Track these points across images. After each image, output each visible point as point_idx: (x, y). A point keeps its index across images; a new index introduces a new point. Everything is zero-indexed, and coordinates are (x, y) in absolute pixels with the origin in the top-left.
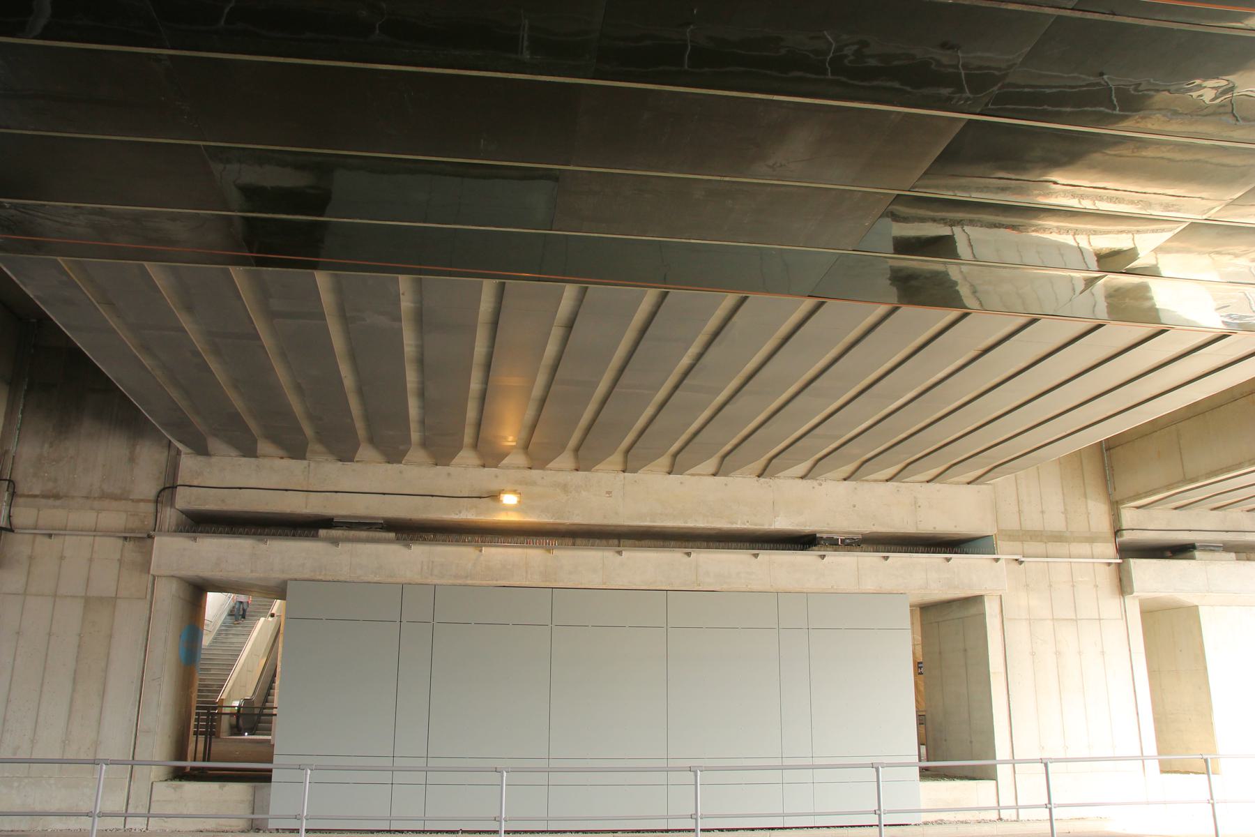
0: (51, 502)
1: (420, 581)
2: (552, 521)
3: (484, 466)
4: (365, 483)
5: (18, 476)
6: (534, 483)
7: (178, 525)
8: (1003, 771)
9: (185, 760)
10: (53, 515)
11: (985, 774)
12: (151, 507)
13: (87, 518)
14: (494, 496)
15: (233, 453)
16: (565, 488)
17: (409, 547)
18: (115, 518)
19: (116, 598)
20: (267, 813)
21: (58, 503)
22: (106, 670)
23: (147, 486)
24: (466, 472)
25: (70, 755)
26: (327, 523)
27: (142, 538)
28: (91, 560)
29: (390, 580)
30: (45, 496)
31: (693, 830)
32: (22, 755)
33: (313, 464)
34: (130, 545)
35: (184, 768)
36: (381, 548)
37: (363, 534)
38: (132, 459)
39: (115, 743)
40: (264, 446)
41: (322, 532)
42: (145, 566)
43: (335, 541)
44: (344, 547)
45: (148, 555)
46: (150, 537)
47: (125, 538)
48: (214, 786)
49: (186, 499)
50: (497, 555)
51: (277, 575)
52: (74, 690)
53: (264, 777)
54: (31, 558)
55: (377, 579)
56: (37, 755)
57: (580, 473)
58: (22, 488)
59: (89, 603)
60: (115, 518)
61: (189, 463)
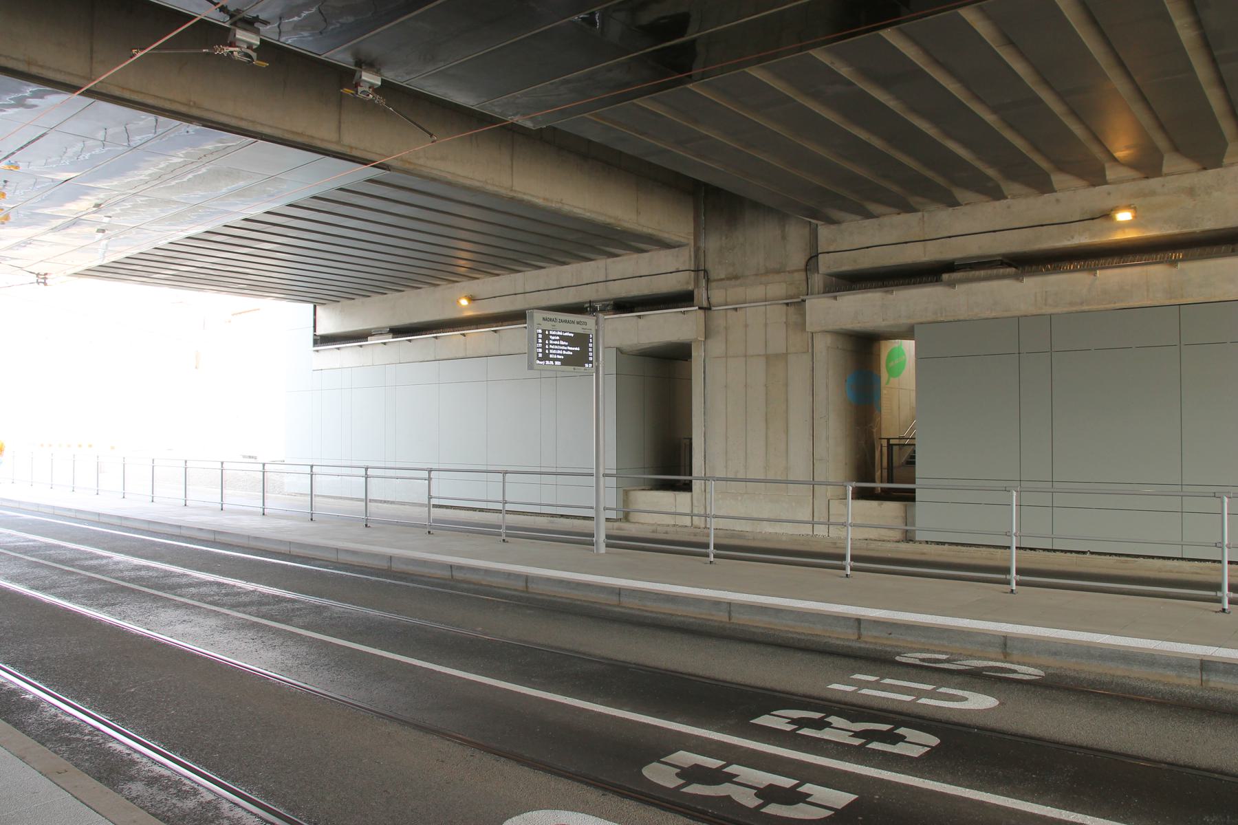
0: (733, 282)
1: (1035, 312)
2: (1176, 231)
3: (1205, 169)
4: (972, 226)
5: (709, 266)
6: (1153, 193)
7: (825, 287)
8: (697, 485)
9: (874, 481)
10: (737, 292)
11: (687, 487)
12: (802, 276)
13: (758, 291)
14: (1107, 215)
15: (858, 218)
16: (1191, 192)
17: (1022, 281)
18: (777, 288)
19: (787, 354)
20: (914, 525)
21: (738, 282)
22: (787, 412)
23: (797, 259)
24: (1071, 196)
25: (771, 476)
26: (950, 267)
27: (796, 304)
28: (766, 325)
29: (1006, 314)
30: (729, 279)
31: (1220, 562)
32: (740, 476)
33: (926, 215)
34: (791, 309)
35: (873, 489)
36: (995, 284)
37: (982, 273)
38: (784, 238)
39: (800, 470)
40: (1057, 179)
41: (945, 276)
42: (802, 326)
43: (951, 284)
44: (961, 289)
45: (803, 315)
46: (804, 301)
47: (787, 304)
48: (874, 504)
49: (827, 264)
50: (1112, 277)
51: (905, 321)
52: (767, 428)
53: (908, 497)
54: (726, 328)
55: (993, 314)
56: (791, 478)
57: (1210, 171)
58: (713, 275)
59: (771, 359)
60: (777, 288)
61: (824, 232)
